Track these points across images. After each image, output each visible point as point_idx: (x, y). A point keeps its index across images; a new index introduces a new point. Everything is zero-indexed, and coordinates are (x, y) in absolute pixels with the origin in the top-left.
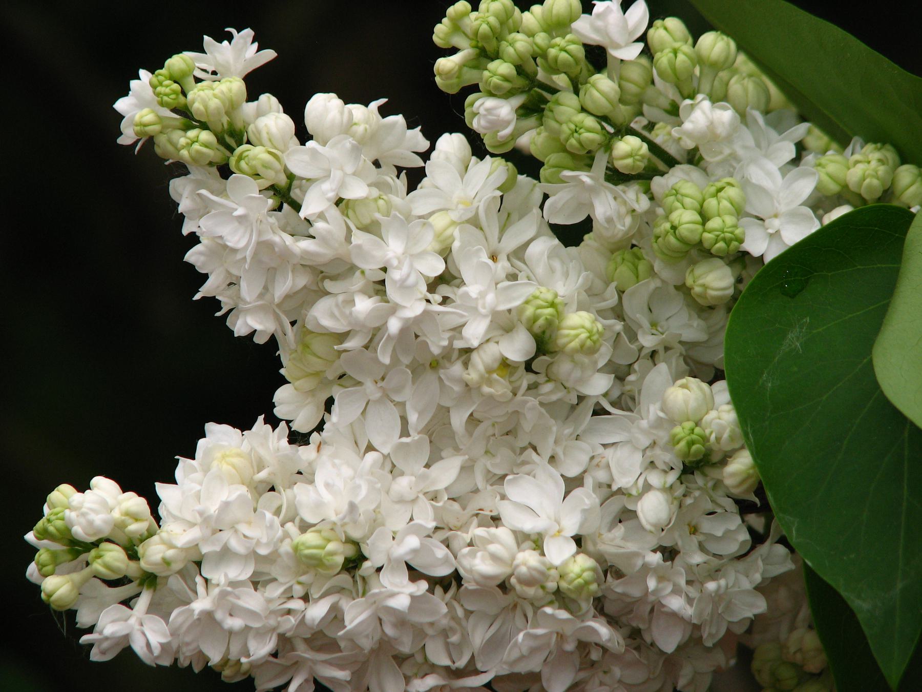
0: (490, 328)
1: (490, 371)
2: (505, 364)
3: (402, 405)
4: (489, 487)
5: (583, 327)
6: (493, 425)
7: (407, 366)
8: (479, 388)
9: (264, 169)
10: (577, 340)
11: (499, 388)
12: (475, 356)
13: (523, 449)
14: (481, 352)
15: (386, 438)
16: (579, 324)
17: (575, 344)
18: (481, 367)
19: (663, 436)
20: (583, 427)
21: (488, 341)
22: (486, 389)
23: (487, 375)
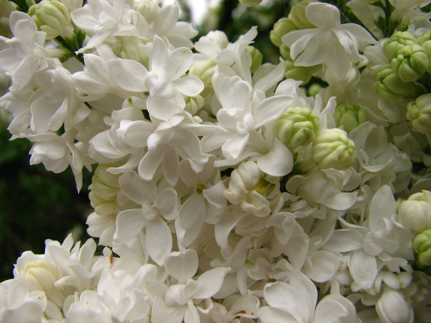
0: (247, 147)
1: (249, 187)
2: (264, 181)
3: (171, 224)
4: (250, 292)
5: (340, 140)
6: (252, 240)
7: (175, 188)
8: (239, 205)
9: (47, 16)
10: (335, 152)
11: (258, 205)
12: (235, 174)
13: (276, 260)
14: (240, 169)
15: (162, 253)
16: (334, 139)
17: (333, 156)
18: (241, 184)
19: (395, 244)
20: (327, 239)
21: (246, 160)
22: (246, 205)
23: (246, 192)
